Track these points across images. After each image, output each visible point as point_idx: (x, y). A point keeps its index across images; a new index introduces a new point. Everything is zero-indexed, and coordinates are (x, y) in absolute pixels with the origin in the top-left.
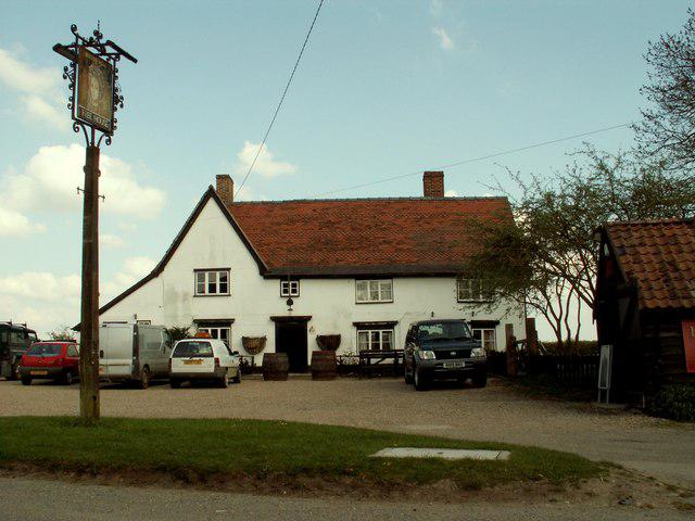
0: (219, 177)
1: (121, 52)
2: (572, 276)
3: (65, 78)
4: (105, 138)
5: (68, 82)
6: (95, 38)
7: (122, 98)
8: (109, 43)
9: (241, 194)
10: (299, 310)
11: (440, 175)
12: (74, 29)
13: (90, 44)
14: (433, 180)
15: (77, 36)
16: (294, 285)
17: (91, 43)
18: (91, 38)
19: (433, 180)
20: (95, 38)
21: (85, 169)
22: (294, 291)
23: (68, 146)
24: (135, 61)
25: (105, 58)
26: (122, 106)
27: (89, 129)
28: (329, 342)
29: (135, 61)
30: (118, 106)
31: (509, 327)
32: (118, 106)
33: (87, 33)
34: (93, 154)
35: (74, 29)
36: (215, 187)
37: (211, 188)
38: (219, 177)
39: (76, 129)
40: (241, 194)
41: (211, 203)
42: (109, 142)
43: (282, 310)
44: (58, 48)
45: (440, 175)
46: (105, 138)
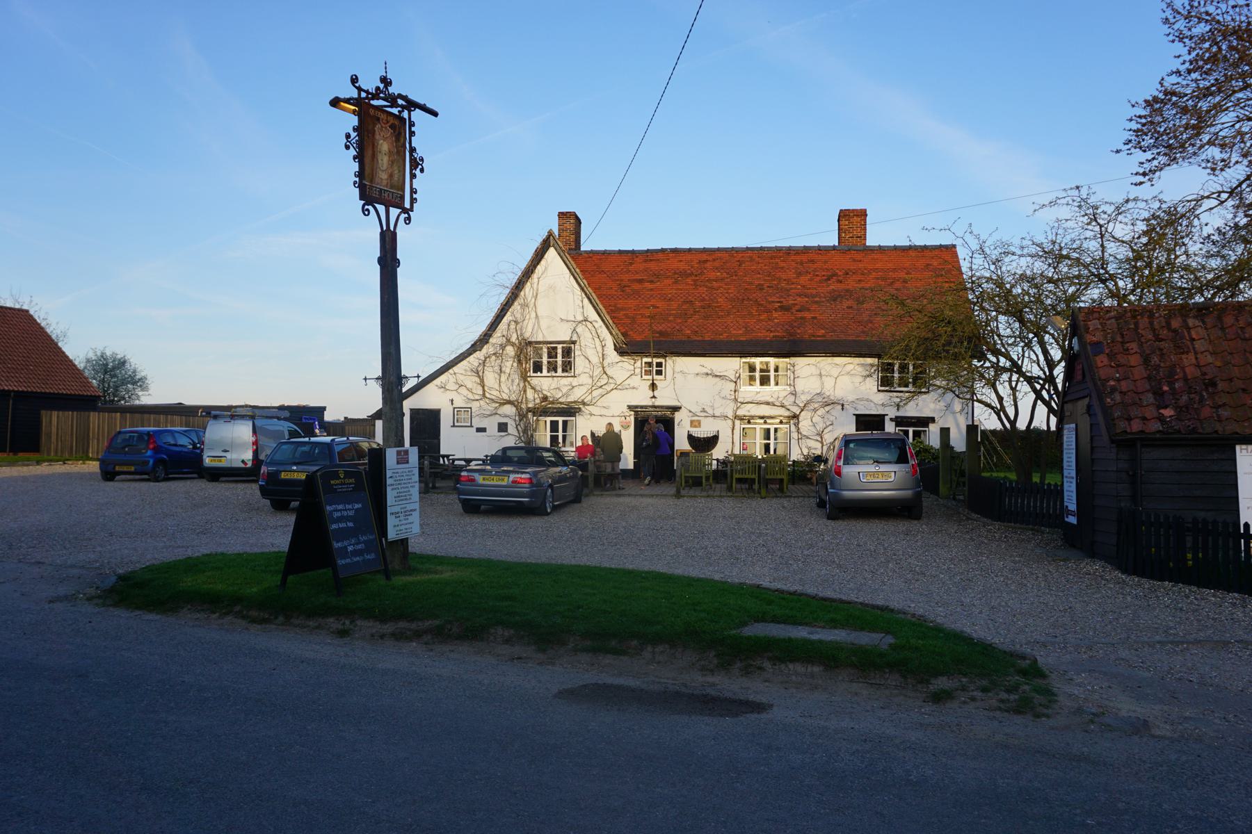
0: (563, 216)
1: (411, 105)
2: (997, 408)
3: (347, 147)
4: (403, 216)
5: (352, 152)
6: (382, 86)
7: (422, 160)
8: (400, 96)
9: (590, 242)
10: (665, 398)
11: (862, 214)
12: (354, 80)
13: (376, 96)
14: (852, 220)
15: (360, 89)
16: (659, 365)
17: (376, 96)
18: (378, 88)
19: (852, 220)
20: (382, 86)
21: (380, 261)
22: (659, 373)
23: (346, 418)
24: (435, 114)
25: (395, 111)
26: (422, 170)
27: (381, 208)
28: (704, 444)
29: (435, 114)
30: (417, 172)
31: (945, 432)
32: (417, 172)
33: (370, 83)
34: (388, 241)
35: (354, 80)
36: (556, 233)
37: (550, 234)
38: (563, 216)
39: (365, 212)
40: (590, 242)
41: (552, 253)
42: (408, 220)
43: (642, 397)
44: (335, 103)
45: (862, 214)
46: (403, 216)
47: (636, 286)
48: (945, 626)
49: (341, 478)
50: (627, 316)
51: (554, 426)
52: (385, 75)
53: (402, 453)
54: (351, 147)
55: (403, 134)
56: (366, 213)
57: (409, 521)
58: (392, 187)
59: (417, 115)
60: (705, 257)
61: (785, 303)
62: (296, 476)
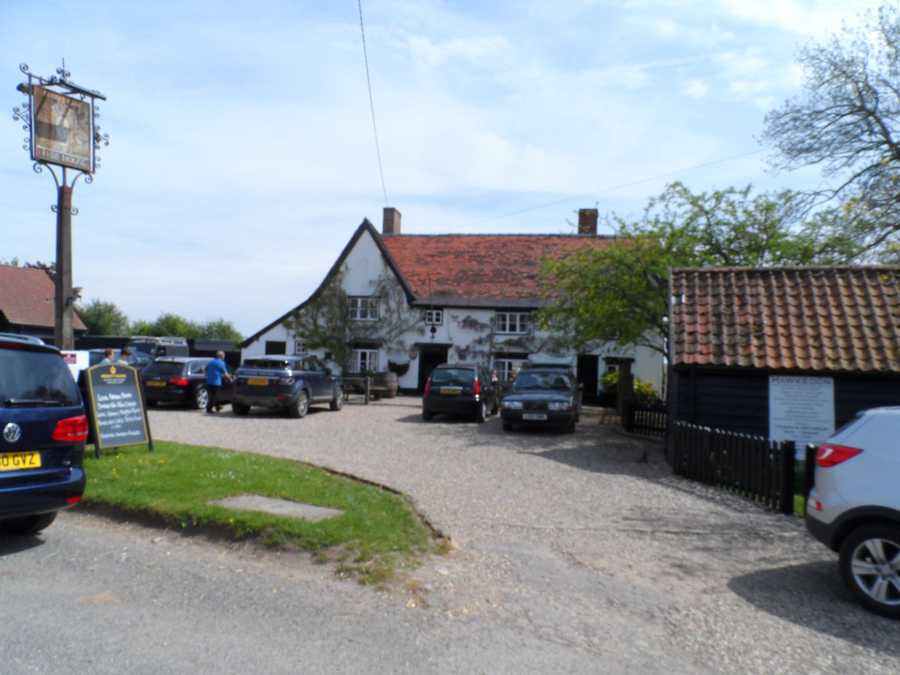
1: (93, 96)
14: (588, 218)
15: (30, 76)
19: (588, 218)
22: (438, 320)
47: (429, 259)
48: (460, 442)
49: (115, 366)
50: (419, 280)
51: (364, 356)
52: (62, 68)
53: (153, 351)
54: (20, 118)
55: (86, 115)
56: (39, 170)
57: (628, 522)
58: (74, 153)
59: (97, 102)
60: (479, 240)
61: (532, 274)
62: (157, 384)
